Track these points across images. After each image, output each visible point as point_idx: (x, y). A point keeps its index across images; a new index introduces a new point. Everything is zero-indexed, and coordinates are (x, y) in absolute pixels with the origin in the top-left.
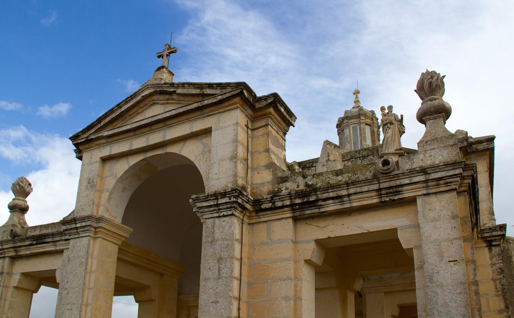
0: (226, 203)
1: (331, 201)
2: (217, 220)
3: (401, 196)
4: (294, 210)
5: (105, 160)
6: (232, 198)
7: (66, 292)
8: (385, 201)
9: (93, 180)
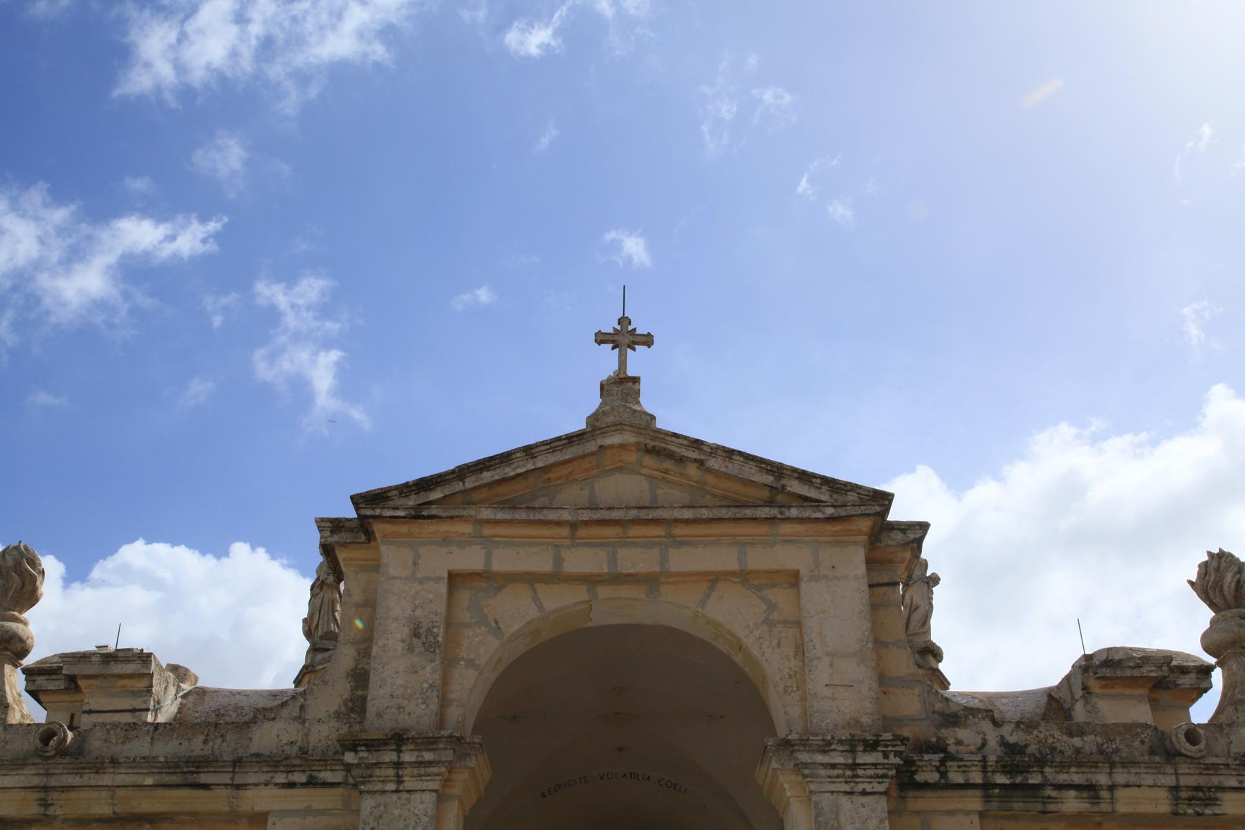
0: (875, 765)
1: (1073, 793)
2: (844, 800)
3: (1217, 810)
4: (987, 798)
5: (455, 579)
6: (892, 756)
8: (334, 610)
9: (429, 630)
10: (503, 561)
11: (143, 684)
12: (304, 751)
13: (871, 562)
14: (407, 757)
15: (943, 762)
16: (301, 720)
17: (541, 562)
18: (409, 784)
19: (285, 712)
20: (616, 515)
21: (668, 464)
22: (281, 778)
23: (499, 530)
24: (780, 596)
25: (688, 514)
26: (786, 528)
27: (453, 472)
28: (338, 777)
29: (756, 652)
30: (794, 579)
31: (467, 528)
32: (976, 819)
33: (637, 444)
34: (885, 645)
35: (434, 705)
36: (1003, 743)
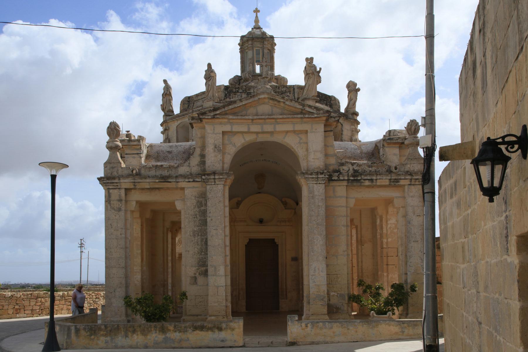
2: (315, 185)
4: (348, 182)
5: (224, 133)
7: (210, 219)
10: (236, 128)
11: (139, 147)
12: (191, 174)
13: (325, 126)
14: (216, 177)
15: (339, 175)
16: (189, 166)
17: (245, 129)
18: (217, 183)
20: (263, 117)
21: (276, 102)
22: (187, 180)
23: (234, 121)
24: (303, 136)
25: (281, 117)
26: (305, 120)
28: (200, 180)
29: (297, 150)
30: (306, 132)
31: (226, 120)
32: (345, 187)
33: (268, 98)
34: (328, 146)
35: (221, 165)
36: (354, 170)
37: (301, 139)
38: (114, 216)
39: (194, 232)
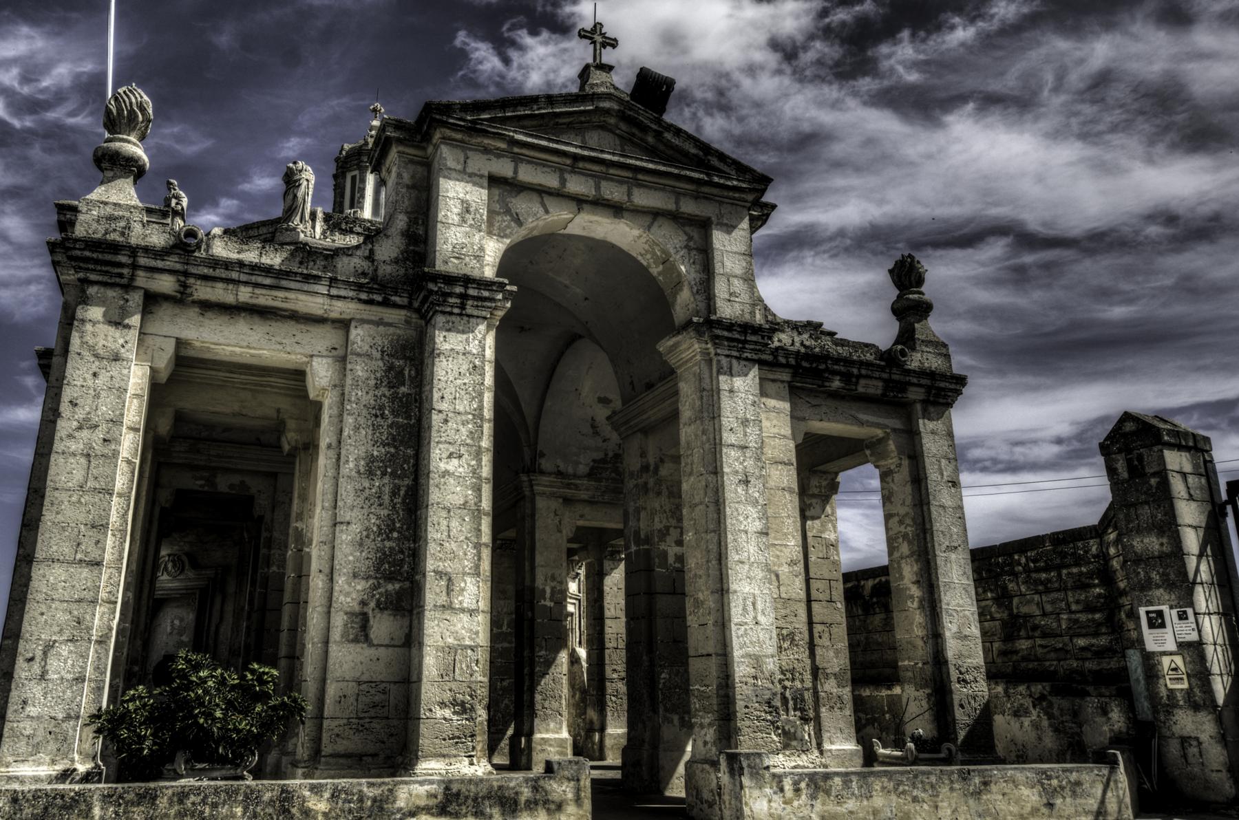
2: (734, 362)
4: (794, 375)
17: (552, 181)
18: (469, 310)
19: (359, 253)
22: (364, 296)
27: (497, 101)
37: (690, 238)
38: (89, 376)
39: (371, 460)
